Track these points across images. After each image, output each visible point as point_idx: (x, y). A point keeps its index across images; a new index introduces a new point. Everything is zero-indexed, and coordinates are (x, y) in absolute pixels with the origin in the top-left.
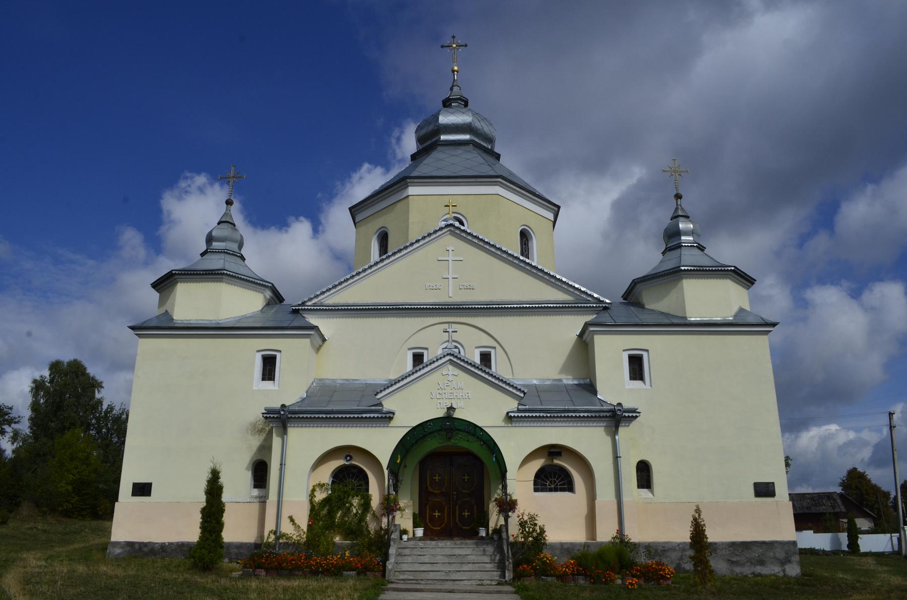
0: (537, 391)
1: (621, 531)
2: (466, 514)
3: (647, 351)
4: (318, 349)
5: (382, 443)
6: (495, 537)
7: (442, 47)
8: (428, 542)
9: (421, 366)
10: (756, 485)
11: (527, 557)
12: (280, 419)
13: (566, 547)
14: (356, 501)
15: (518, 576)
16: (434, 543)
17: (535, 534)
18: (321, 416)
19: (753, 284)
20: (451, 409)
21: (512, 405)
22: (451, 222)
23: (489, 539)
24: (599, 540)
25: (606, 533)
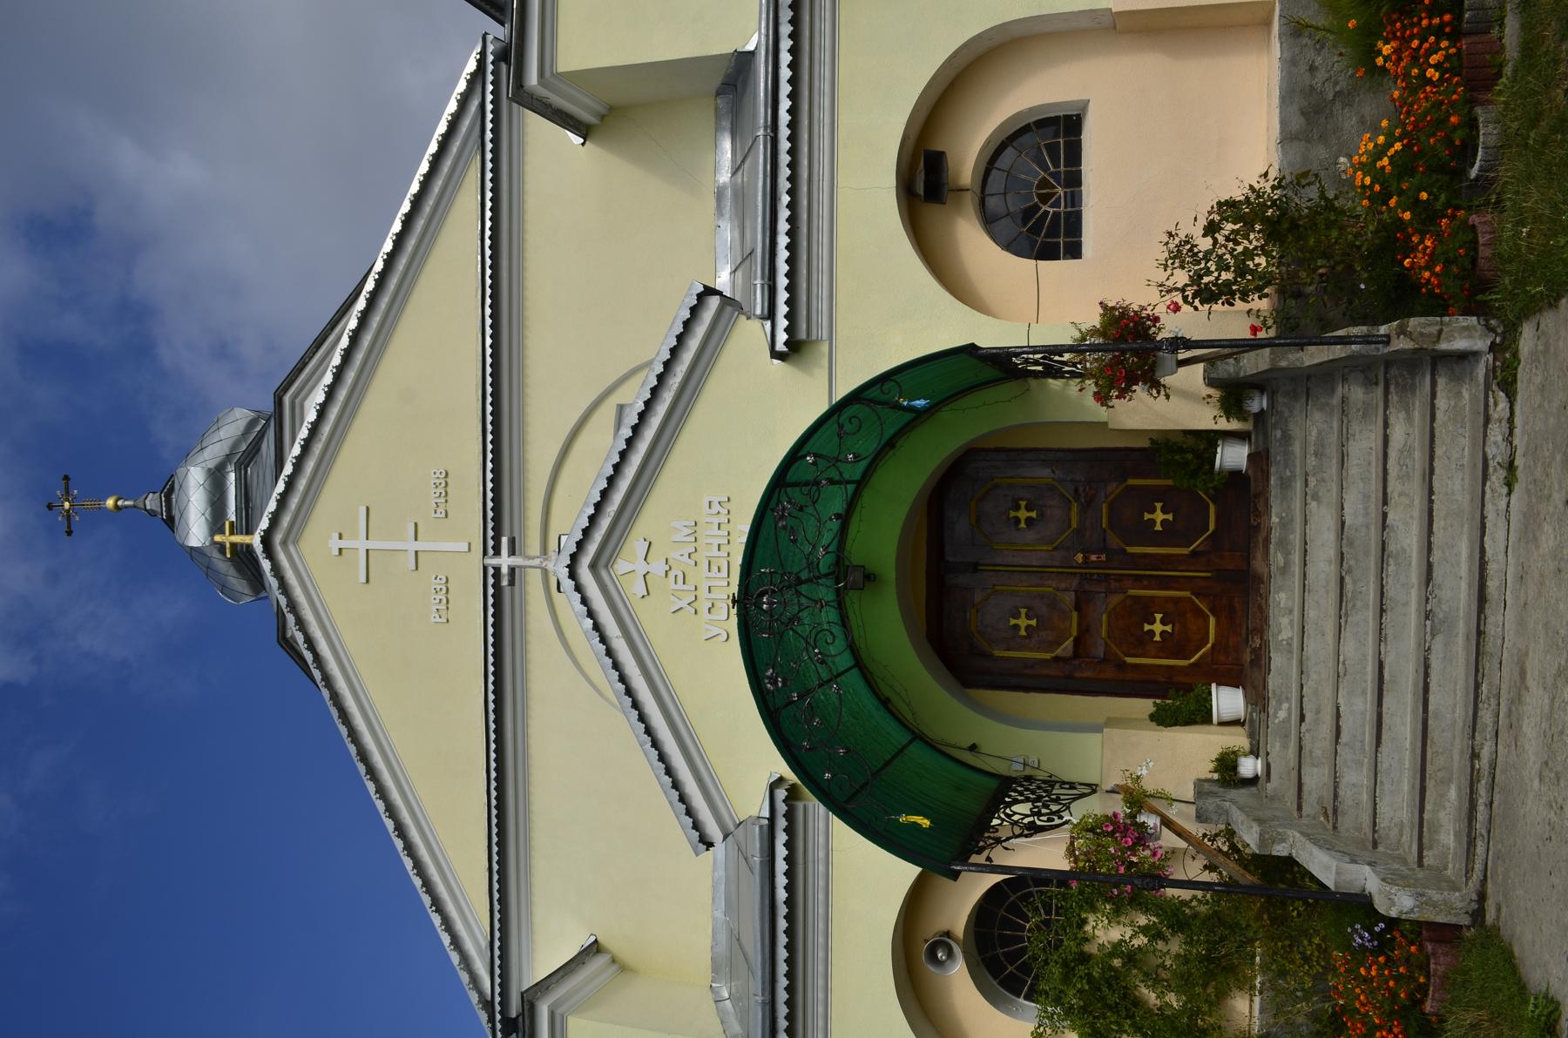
2: (1159, 516)
4: (620, 966)
6: (1257, 403)
7: (69, 533)
11: (1348, 270)
13: (1298, 122)
14: (1107, 932)
15: (1471, 291)
16: (1277, 660)
23: (1261, 435)
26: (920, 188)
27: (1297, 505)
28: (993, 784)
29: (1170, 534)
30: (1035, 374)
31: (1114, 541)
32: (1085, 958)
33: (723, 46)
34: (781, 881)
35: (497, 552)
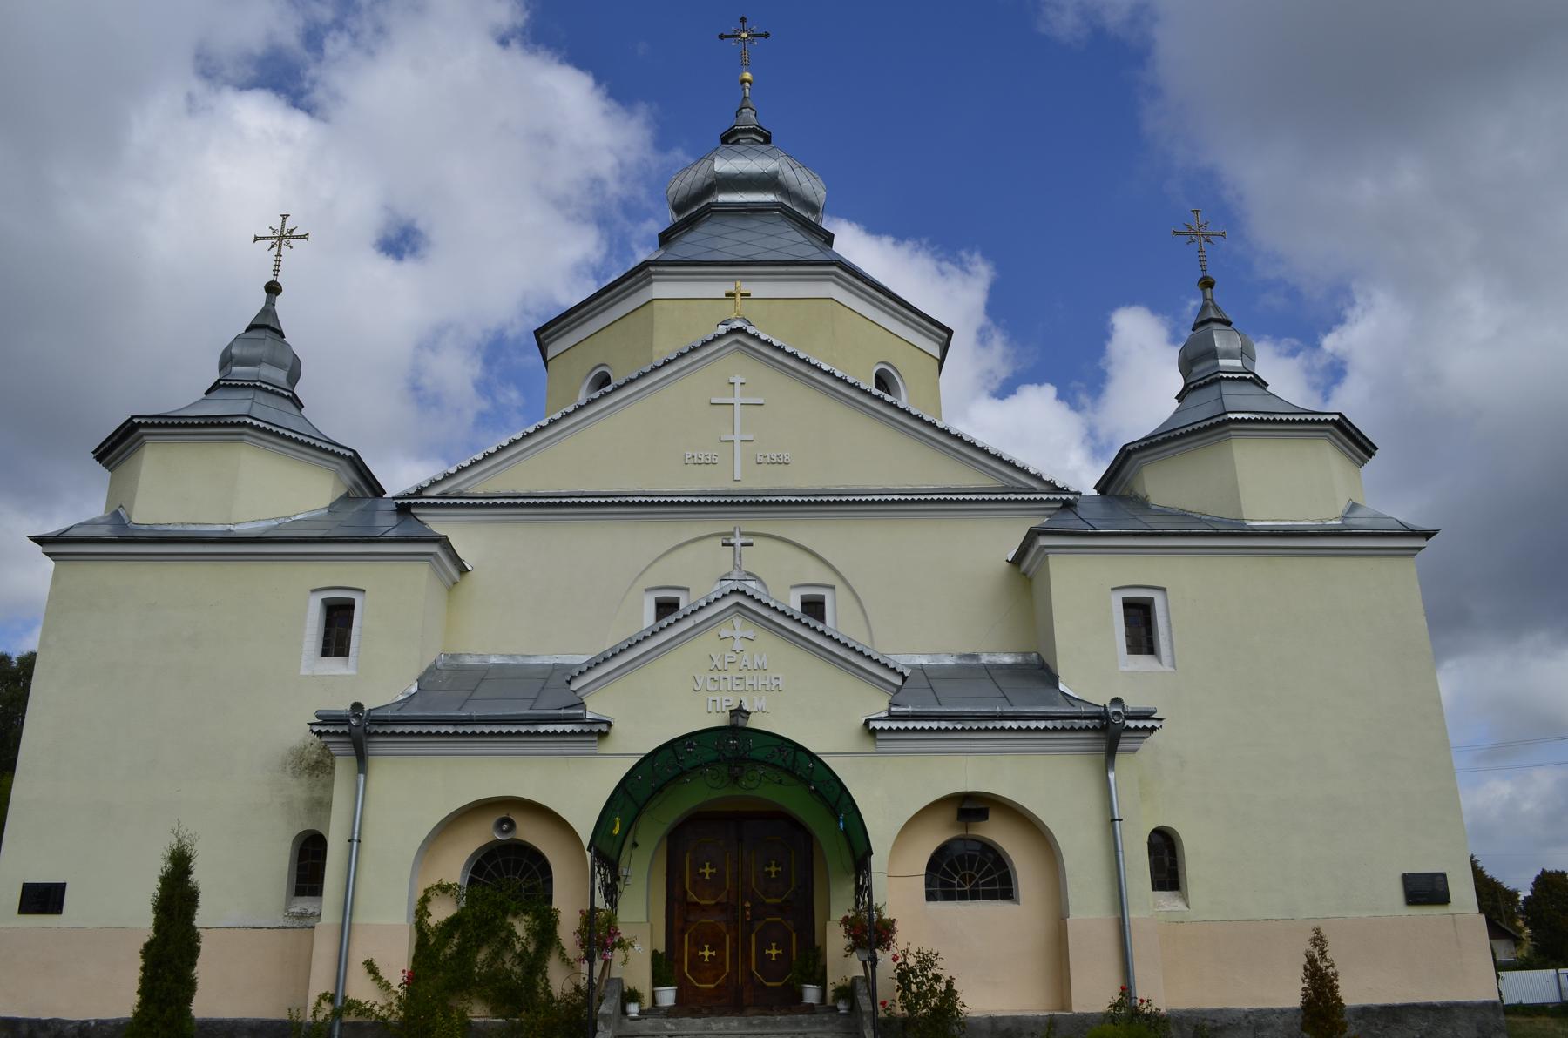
0: (927, 676)
1: (1126, 990)
2: (774, 952)
3: (1163, 589)
5: (579, 789)
7: (722, 37)
8: (687, 1020)
9: (671, 619)
10: (1407, 879)
12: (355, 734)
14: (520, 927)
16: (699, 1022)
17: (933, 1002)
18: (443, 729)
19: (1370, 455)
20: (739, 712)
21: (876, 704)
22: (738, 324)
24: (1076, 1009)
25: (1093, 994)
26: (966, 806)
27: (787, 1030)
28: (614, 857)
29: (763, 959)
30: (857, 880)
31: (758, 925)
32: (505, 913)
33: (1062, 669)
34: (551, 728)
35: (742, 534)
